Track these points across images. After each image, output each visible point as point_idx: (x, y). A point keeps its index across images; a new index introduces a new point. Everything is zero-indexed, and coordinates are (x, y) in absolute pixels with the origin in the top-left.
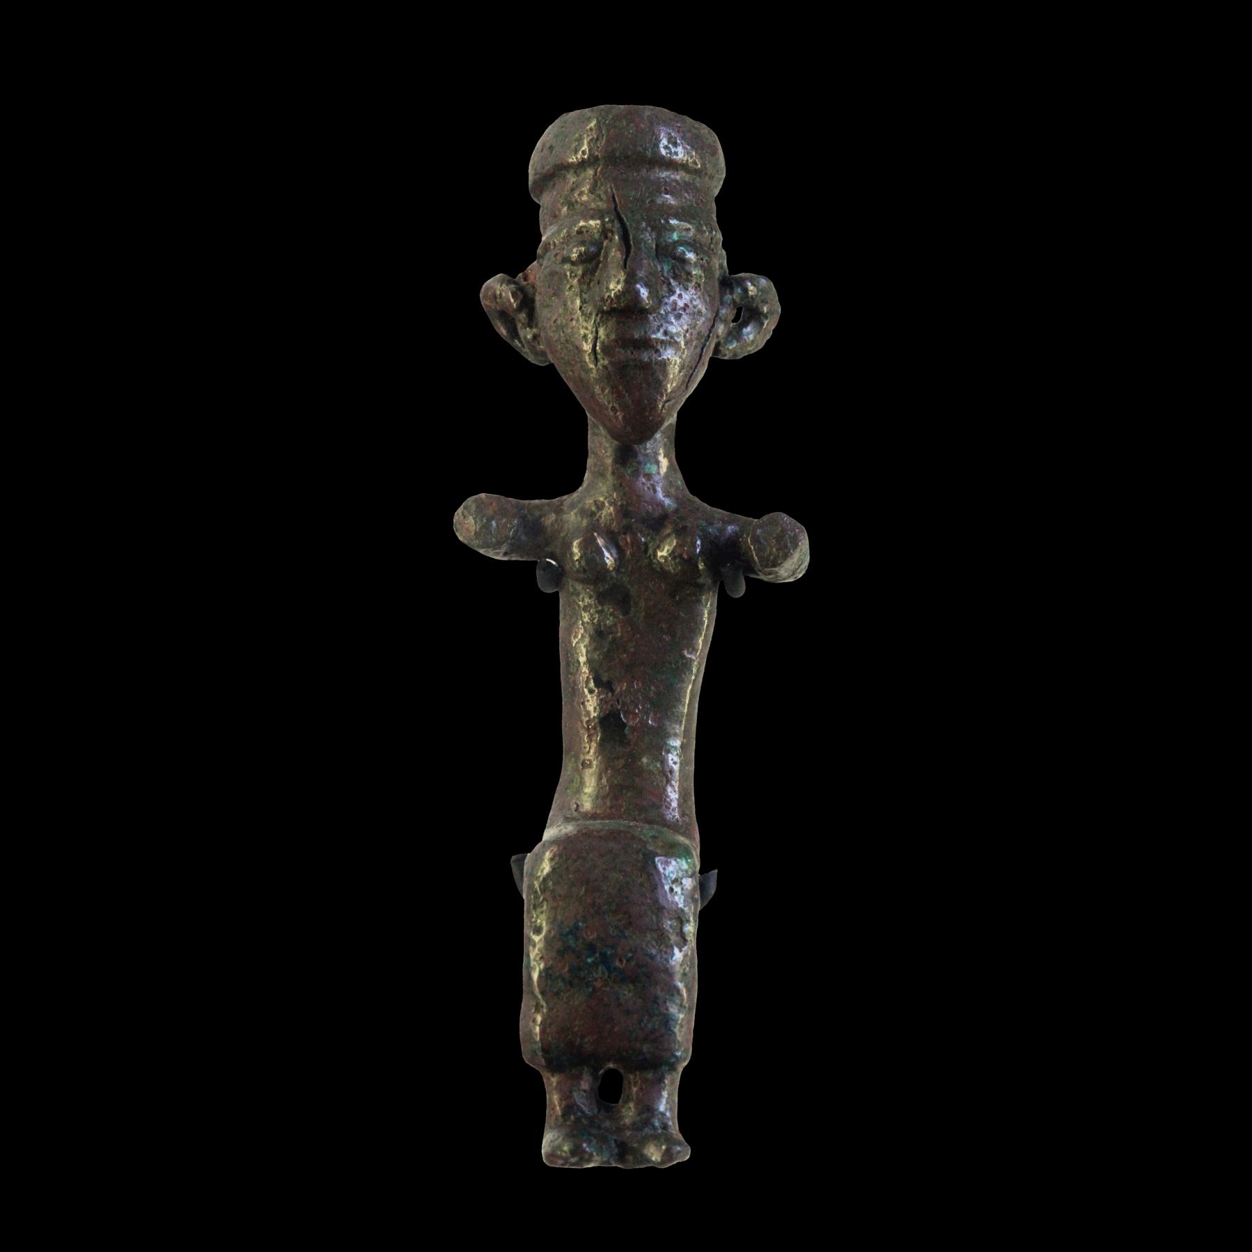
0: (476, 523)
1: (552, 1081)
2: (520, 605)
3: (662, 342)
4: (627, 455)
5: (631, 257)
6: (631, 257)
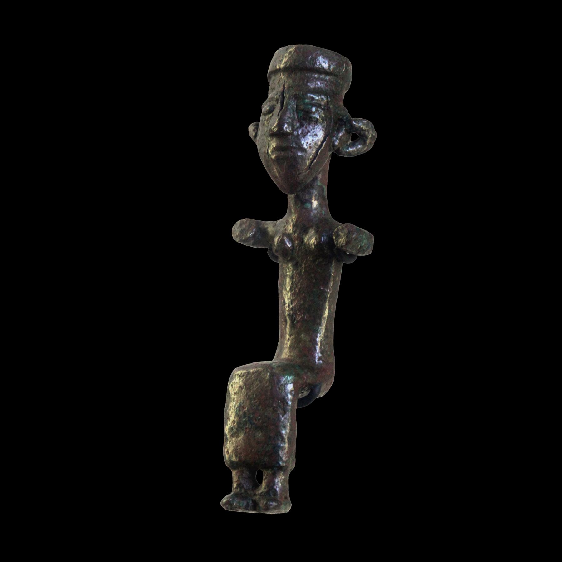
0: (241, 231)
1: (234, 473)
2: (260, 267)
3: (294, 148)
4: (302, 202)
5: (304, 115)
6: (304, 115)
